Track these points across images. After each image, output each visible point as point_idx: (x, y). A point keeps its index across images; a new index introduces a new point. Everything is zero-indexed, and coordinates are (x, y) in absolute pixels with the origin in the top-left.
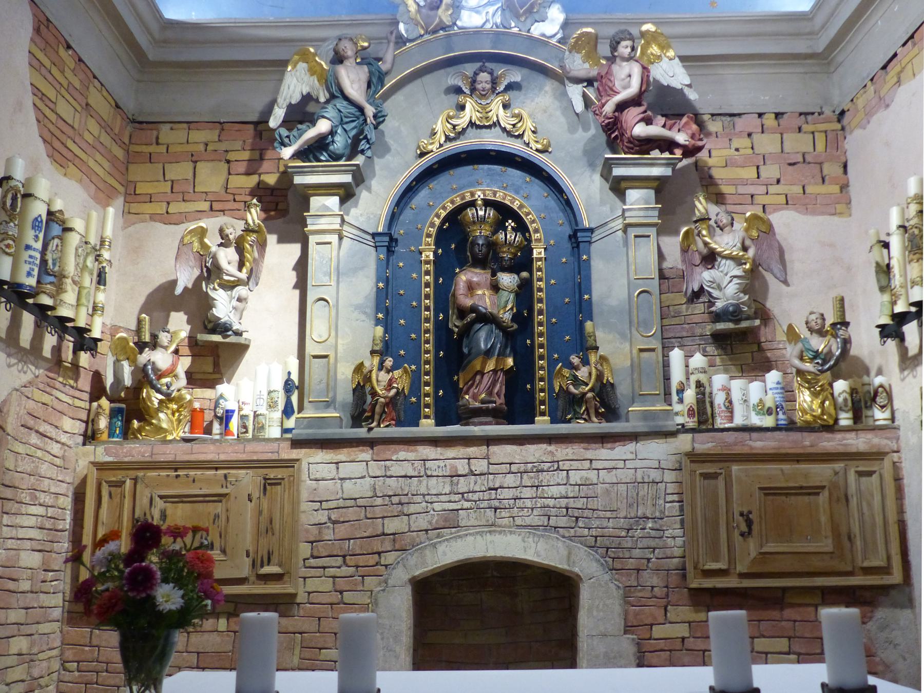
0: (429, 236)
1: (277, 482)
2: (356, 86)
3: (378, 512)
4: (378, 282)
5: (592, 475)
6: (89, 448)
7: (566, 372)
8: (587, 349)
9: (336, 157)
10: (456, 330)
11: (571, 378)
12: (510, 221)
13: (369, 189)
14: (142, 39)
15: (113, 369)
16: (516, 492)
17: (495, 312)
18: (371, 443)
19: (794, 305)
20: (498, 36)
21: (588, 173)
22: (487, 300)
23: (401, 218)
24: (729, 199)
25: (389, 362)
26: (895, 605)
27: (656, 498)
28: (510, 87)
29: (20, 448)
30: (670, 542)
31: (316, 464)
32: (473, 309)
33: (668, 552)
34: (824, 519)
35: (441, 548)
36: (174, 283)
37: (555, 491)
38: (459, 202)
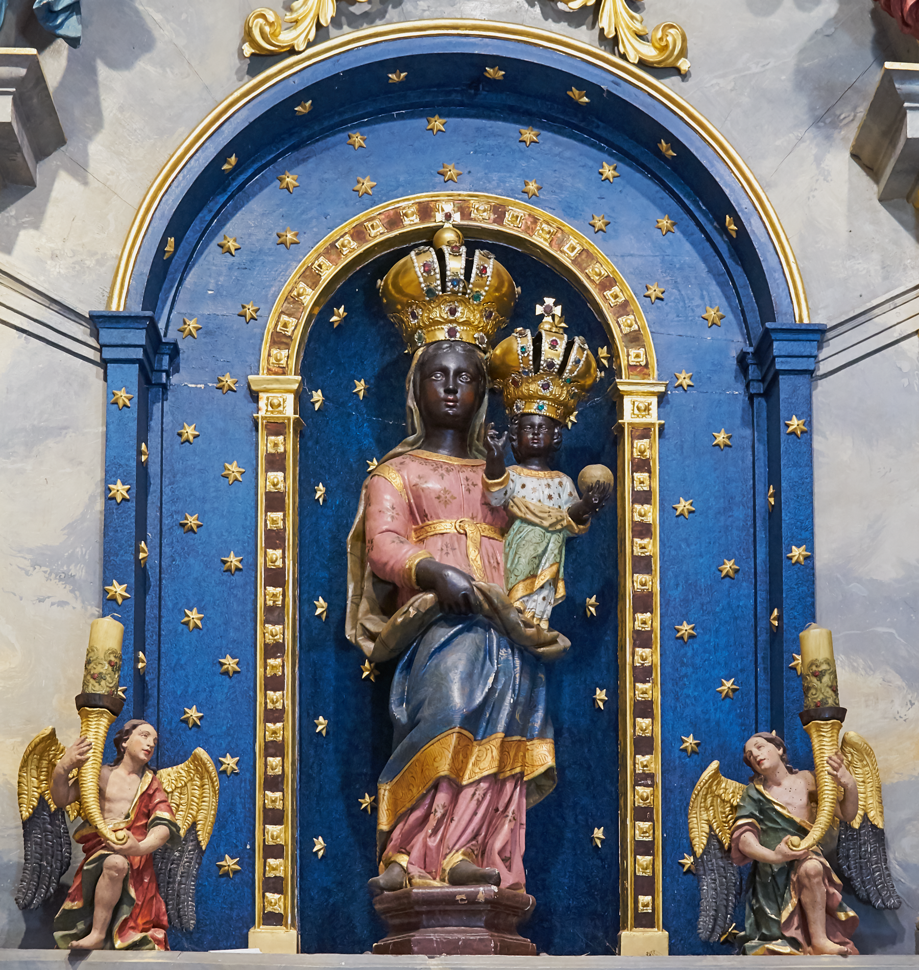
0: (280, 340)
4: (109, 477)
7: (731, 789)
8: (807, 717)
10: (368, 646)
11: (750, 808)
12: (549, 301)
13: (80, 170)
17: (497, 587)
21: (809, 148)
22: (473, 554)
23: (190, 279)
25: (142, 738)
32: (428, 578)
38: (378, 233)
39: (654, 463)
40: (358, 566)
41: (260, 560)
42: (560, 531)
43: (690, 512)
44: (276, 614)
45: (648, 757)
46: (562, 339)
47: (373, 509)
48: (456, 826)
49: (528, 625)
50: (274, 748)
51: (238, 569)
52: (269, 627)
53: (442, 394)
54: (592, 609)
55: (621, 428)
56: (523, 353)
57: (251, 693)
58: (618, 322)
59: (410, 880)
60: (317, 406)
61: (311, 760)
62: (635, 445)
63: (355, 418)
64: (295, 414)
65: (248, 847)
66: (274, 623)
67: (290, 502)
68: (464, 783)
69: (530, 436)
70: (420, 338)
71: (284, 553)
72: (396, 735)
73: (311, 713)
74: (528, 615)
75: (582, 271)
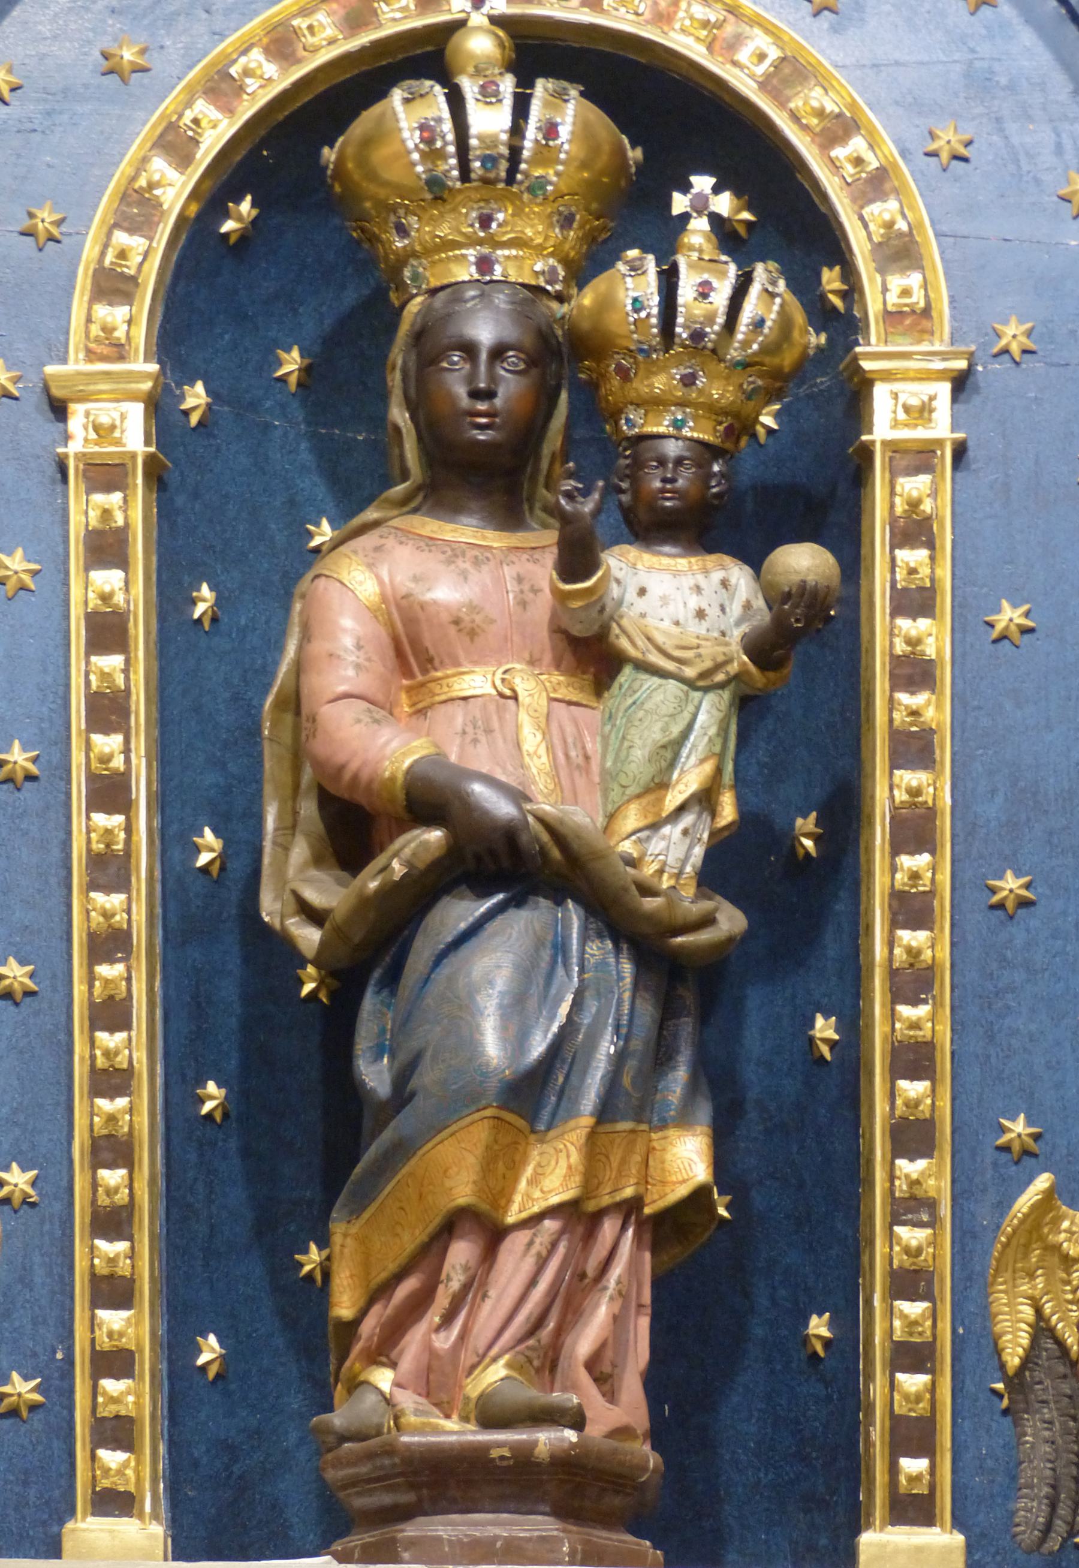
0: (113, 286)
12: (702, 183)
17: (582, 816)
22: (531, 739)
32: (429, 799)
39: (942, 526)
40: (287, 764)
41: (77, 757)
42: (721, 686)
43: (1026, 631)
44: (112, 870)
45: (921, 1164)
46: (723, 274)
47: (317, 647)
48: (494, 1308)
49: (646, 890)
50: (113, 1149)
51: (30, 778)
52: (98, 897)
53: (465, 402)
54: (808, 843)
55: (866, 453)
56: (637, 311)
57: (62, 1037)
58: (861, 218)
59: (396, 1418)
60: (194, 419)
61: (191, 1174)
62: (898, 489)
63: (278, 433)
64: (147, 443)
65: (59, 1356)
66: (108, 889)
67: (139, 632)
68: (511, 1219)
69: (658, 484)
70: (416, 277)
71: (127, 741)
72: (367, 1123)
73: (191, 1074)
74: (649, 870)
75: (782, 104)
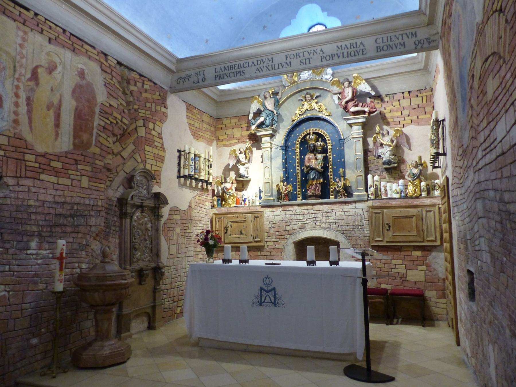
1: (258, 217)
2: (270, 105)
3: (284, 224)
5: (343, 213)
6: (213, 209)
9: (268, 126)
13: (279, 133)
14: (214, 97)
15: (218, 189)
16: (321, 219)
18: (281, 206)
19: (411, 157)
20: (312, 82)
24: (391, 124)
26: (438, 251)
27: (362, 219)
28: (317, 97)
29: (195, 211)
30: (366, 232)
31: (267, 212)
32: (309, 166)
33: (365, 235)
34: (414, 225)
35: (301, 234)
36: (228, 165)
37: (332, 218)
